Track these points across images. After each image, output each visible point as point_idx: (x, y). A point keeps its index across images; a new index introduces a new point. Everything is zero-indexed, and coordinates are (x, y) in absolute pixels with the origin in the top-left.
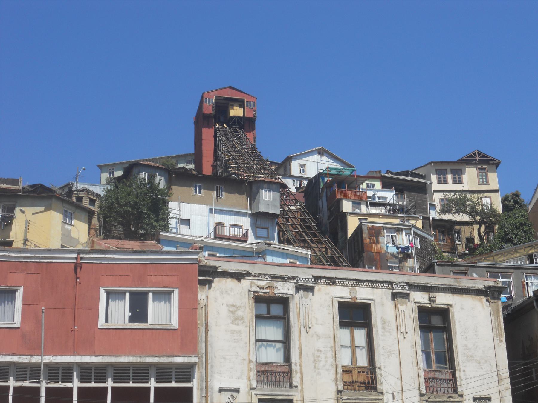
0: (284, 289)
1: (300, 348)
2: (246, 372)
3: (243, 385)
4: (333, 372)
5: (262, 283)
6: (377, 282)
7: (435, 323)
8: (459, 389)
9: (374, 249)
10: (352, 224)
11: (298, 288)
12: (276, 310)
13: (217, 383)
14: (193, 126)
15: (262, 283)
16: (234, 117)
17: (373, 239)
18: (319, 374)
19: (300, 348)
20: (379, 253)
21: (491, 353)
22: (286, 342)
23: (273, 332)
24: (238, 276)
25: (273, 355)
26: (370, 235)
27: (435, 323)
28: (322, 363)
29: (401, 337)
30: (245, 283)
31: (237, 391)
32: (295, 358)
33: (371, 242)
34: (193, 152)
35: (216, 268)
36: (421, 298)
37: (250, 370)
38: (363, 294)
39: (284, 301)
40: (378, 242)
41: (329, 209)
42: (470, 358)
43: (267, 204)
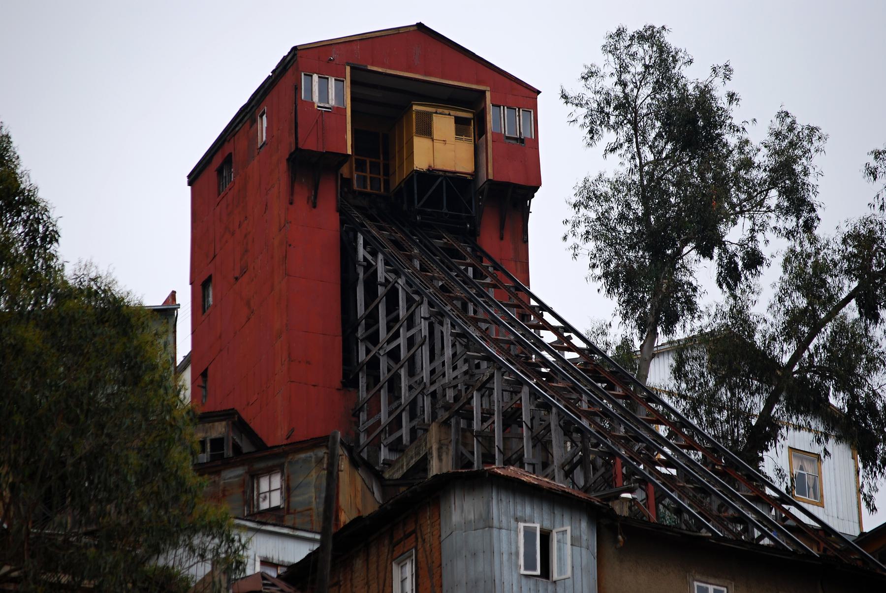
14: (182, 198)
16: (431, 176)
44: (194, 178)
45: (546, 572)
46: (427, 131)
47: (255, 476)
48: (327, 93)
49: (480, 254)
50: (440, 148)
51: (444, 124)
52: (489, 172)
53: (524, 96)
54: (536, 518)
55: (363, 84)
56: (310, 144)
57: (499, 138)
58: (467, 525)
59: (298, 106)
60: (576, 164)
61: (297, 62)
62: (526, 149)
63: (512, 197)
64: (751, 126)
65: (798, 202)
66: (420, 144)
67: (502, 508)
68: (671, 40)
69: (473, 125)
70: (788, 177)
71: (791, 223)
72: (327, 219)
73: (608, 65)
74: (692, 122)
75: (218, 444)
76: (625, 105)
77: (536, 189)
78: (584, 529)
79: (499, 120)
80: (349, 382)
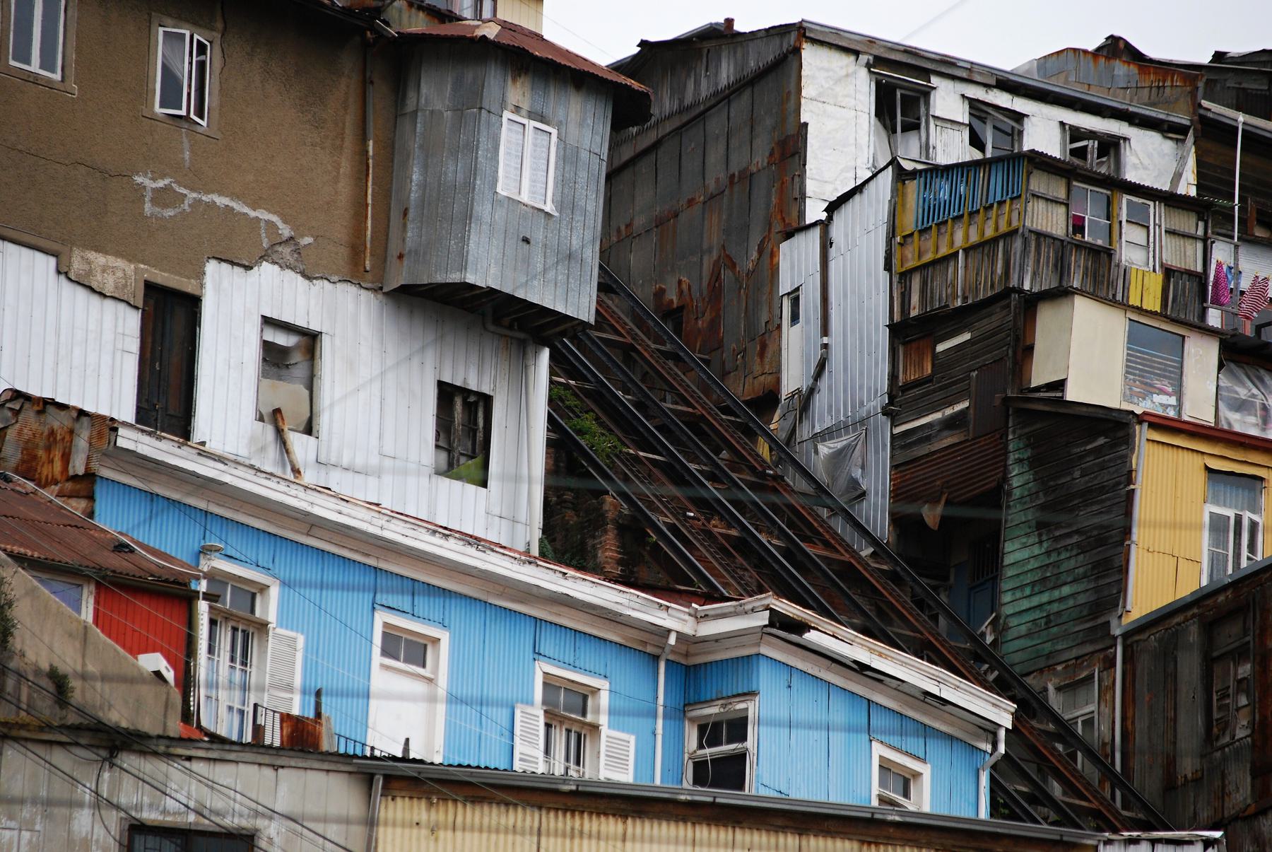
41: (907, 333)
43: (524, 229)
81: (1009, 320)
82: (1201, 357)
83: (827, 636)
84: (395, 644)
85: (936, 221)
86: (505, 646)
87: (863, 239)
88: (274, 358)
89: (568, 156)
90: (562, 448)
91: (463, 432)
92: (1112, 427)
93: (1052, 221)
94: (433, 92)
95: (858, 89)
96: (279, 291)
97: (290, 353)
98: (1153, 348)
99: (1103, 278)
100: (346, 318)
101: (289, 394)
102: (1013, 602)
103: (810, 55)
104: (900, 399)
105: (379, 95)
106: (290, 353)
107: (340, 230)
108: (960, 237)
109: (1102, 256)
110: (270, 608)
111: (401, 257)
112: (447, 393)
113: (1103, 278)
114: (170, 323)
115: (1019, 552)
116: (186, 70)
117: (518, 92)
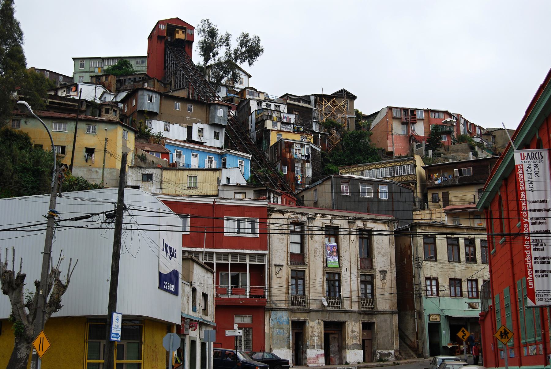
0: (303, 218)
1: (309, 247)
2: (286, 257)
3: (284, 263)
4: (322, 258)
5: (293, 216)
6: (342, 216)
7: (366, 237)
8: (374, 268)
9: (288, 156)
10: (274, 139)
11: (308, 218)
12: (298, 228)
13: (274, 262)
14: (147, 41)
15: (293, 216)
16: (178, 39)
17: (288, 150)
18: (316, 259)
19: (309, 247)
20: (290, 158)
21: (388, 251)
22: (302, 244)
23: (297, 238)
24: (282, 212)
25: (296, 249)
26: (286, 147)
27: (366, 237)
28: (318, 254)
29: (351, 243)
30: (286, 216)
31: (282, 266)
32: (306, 251)
33: (286, 152)
34: (146, 55)
35: (274, 208)
36: (360, 224)
37: (288, 257)
38: (336, 222)
39: (302, 224)
40: (290, 151)
41: (257, 124)
42: (379, 253)
43: (220, 118)
44: (148, 38)
45: (151, 101)
46: (178, 33)
47: (144, 83)
48: (163, 27)
49: (185, 51)
50: (180, 35)
51: (180, 32)
52: (187, 39)
53: (192, 28)
54: (150, 94)
55: (169, 26)
56: (160, 35)
57: (188, 34)
58: (141, 95)
59: (159, 29)
60: (198, 38)
61: (159, 23)
62: (192, 36)
63: (191, 42)
64: (221, 34)
65: (228, 45)
66: (177, 35)
67: (145, 93)
68: (210, 21)
69: (184, 32)
70: (227, 41)
71: (227, 47)
72: (163, 45)
73: (201, 24)
74: (212, 33)
75: (143, 78)
76: (204, 30)
77: (193, 42)
78: (158, 96)
79: (188, 31)
80: (165, 69)
81: (263, 122)
82: (279, 124)
83: (232, 151)
84: (193, 155)
85: (258, 114)
86: (204, 155)
87: (253, 116)
88: (199, 131)
89: (224, 112)
90: (226, 137)
91: (217, 136)
92: (269, 130)
93: (267, 114)
94: (212, 108)
95: (256, 103)
96: (200, 125)
97: (201, 131)
98: (275, 124)
99: (271, 118)
100: (206, 127)
101: (201, 134)
102: (264, 146)
103: (251, 101)
104: (256, 129)
105: (208, 108)
106: (201, 131)
107: (205, 120)
108: (260, 115)
109: (271, 116)
110: (182, 153)
111: (106, 130)
112: (215, 132)
113: (271, 118)
114: (190, 129)
115: (264, 141)
116: (191, 108)
117: (219, 107)
